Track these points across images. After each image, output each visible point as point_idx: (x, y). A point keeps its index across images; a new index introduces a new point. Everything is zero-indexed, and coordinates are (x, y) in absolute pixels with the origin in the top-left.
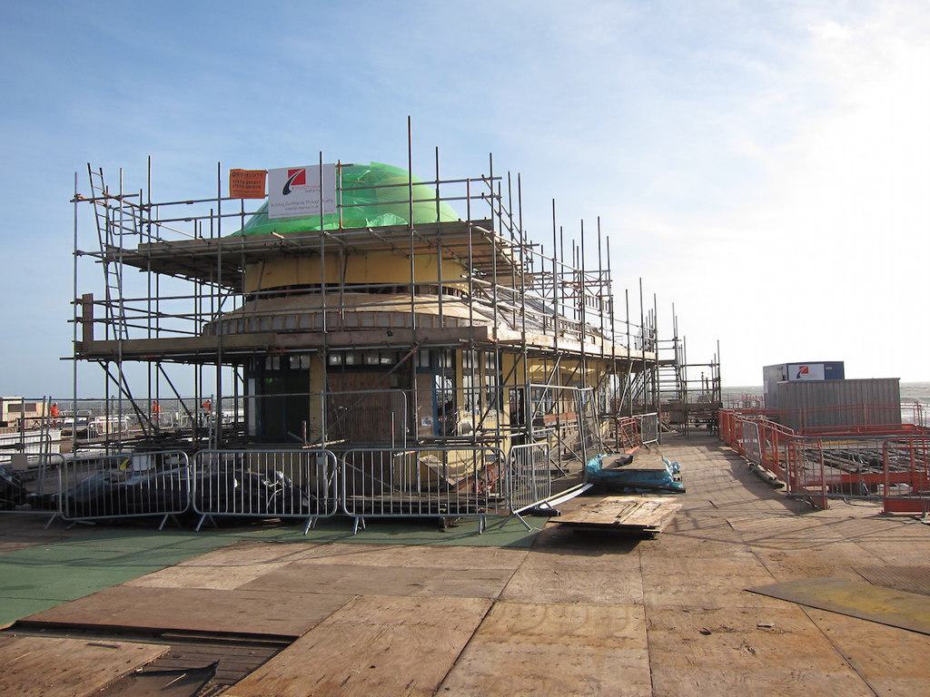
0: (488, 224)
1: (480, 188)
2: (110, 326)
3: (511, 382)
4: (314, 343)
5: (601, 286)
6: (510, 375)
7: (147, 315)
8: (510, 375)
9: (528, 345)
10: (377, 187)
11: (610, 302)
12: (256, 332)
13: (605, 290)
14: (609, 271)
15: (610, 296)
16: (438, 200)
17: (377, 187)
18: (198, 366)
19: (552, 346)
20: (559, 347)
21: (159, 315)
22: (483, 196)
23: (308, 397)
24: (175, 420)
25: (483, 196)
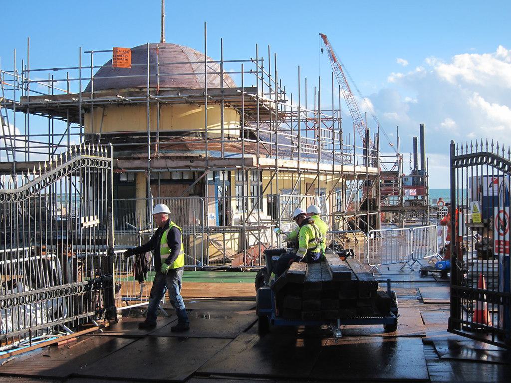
0: (254, 90)
1: (252, 66)
2: (27, 154)
3: (268, 192)
4: (142, 166)
5: (333, 121)
6: (265, 189)
7: (17, 138)
8: (265, 189)
9: (280, 167)
10: (198, 74)
11: (341, 133)
12: (177, 181)
13: (336, 124)
14: (340, 110)
15: (341, 130)
16: (68, 80)
17: (198, 74)
18: (27, 161)
19: (297, 167)
20: (301, 167)
21: (26, 141)
22: (251, 72)
23: (135, 202)
24: (127, 254)
25: (251, 72)
